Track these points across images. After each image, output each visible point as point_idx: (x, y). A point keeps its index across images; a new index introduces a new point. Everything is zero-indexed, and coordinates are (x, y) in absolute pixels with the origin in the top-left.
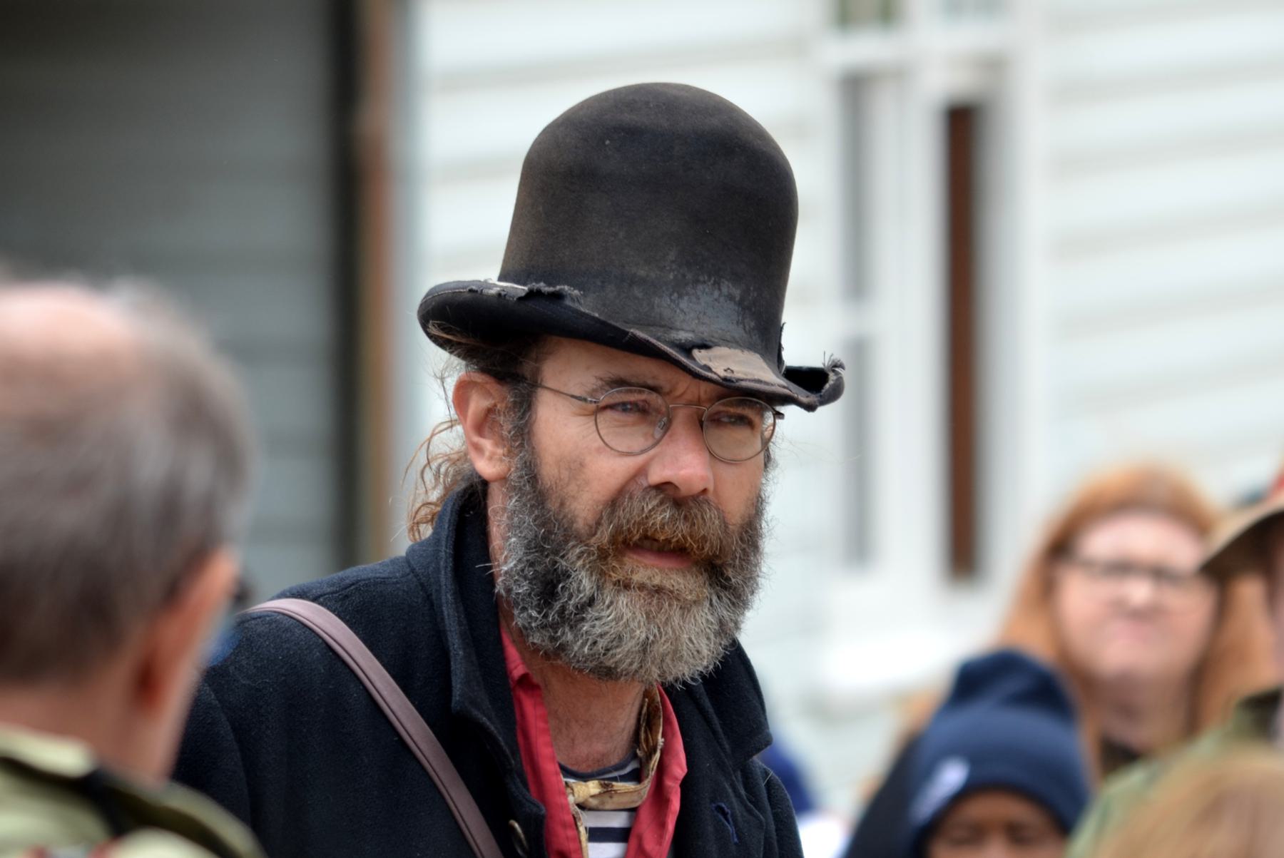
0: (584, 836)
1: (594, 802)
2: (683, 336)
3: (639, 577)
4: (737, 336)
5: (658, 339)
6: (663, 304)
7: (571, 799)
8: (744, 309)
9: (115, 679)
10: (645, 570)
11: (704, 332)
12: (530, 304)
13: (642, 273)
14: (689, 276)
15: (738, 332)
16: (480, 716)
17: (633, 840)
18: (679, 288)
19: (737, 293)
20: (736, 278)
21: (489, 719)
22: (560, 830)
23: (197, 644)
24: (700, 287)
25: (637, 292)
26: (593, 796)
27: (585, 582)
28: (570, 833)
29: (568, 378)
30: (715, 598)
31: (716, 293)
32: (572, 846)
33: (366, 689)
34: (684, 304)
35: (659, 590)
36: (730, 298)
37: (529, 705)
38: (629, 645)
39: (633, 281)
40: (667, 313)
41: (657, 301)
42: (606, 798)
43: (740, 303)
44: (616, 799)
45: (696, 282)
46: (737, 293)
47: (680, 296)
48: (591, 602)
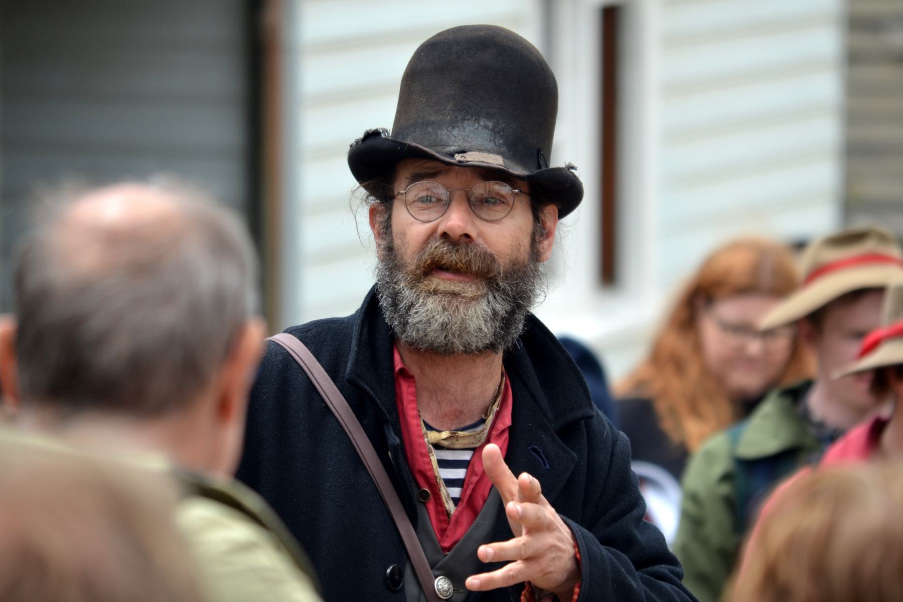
0: (435, 464)
1: (446, 443)
2: (452, 149)
3: (442, 287)
4: (489, 148)
5: (439, 153)
6: (443, 134)
7: (426, 440)
8: (495, 133)
9: (206, 405)
10: (441, 282)
11: (466, 145)
12: (370, 142)
13: (433, 119)
14: (459, 117)
15: (490, 145)
16: (362, 384)
17: (470, 467)
18: (453, 124)
19: (490, 124)
20: (489, 116)
21: (372, 389)
22: (419, 457)
23: (241, 376)
24: (466, 122)
25: (430, 130)
26: (444, 439)
27: (408, 295)
28: (426, 460)
29: (409, 192)
30: (491, 297)
31: (476, 125)
32: (427, 467)
33: (308, 377)
34: (455, 132)
35: (454, 295)
36: (486, 127)
37: (405, 389)
38: (435, 326)
39: (429, 124)
40: (445, 138)
41: (440, 132)
42: (454, 441)
43: (492, 130)
44: (460, 441)
45: (464, 119)
46: (490, 124)
47: (453, 128)
48: (412, 305)
